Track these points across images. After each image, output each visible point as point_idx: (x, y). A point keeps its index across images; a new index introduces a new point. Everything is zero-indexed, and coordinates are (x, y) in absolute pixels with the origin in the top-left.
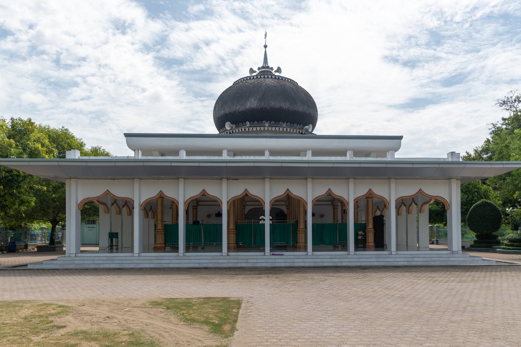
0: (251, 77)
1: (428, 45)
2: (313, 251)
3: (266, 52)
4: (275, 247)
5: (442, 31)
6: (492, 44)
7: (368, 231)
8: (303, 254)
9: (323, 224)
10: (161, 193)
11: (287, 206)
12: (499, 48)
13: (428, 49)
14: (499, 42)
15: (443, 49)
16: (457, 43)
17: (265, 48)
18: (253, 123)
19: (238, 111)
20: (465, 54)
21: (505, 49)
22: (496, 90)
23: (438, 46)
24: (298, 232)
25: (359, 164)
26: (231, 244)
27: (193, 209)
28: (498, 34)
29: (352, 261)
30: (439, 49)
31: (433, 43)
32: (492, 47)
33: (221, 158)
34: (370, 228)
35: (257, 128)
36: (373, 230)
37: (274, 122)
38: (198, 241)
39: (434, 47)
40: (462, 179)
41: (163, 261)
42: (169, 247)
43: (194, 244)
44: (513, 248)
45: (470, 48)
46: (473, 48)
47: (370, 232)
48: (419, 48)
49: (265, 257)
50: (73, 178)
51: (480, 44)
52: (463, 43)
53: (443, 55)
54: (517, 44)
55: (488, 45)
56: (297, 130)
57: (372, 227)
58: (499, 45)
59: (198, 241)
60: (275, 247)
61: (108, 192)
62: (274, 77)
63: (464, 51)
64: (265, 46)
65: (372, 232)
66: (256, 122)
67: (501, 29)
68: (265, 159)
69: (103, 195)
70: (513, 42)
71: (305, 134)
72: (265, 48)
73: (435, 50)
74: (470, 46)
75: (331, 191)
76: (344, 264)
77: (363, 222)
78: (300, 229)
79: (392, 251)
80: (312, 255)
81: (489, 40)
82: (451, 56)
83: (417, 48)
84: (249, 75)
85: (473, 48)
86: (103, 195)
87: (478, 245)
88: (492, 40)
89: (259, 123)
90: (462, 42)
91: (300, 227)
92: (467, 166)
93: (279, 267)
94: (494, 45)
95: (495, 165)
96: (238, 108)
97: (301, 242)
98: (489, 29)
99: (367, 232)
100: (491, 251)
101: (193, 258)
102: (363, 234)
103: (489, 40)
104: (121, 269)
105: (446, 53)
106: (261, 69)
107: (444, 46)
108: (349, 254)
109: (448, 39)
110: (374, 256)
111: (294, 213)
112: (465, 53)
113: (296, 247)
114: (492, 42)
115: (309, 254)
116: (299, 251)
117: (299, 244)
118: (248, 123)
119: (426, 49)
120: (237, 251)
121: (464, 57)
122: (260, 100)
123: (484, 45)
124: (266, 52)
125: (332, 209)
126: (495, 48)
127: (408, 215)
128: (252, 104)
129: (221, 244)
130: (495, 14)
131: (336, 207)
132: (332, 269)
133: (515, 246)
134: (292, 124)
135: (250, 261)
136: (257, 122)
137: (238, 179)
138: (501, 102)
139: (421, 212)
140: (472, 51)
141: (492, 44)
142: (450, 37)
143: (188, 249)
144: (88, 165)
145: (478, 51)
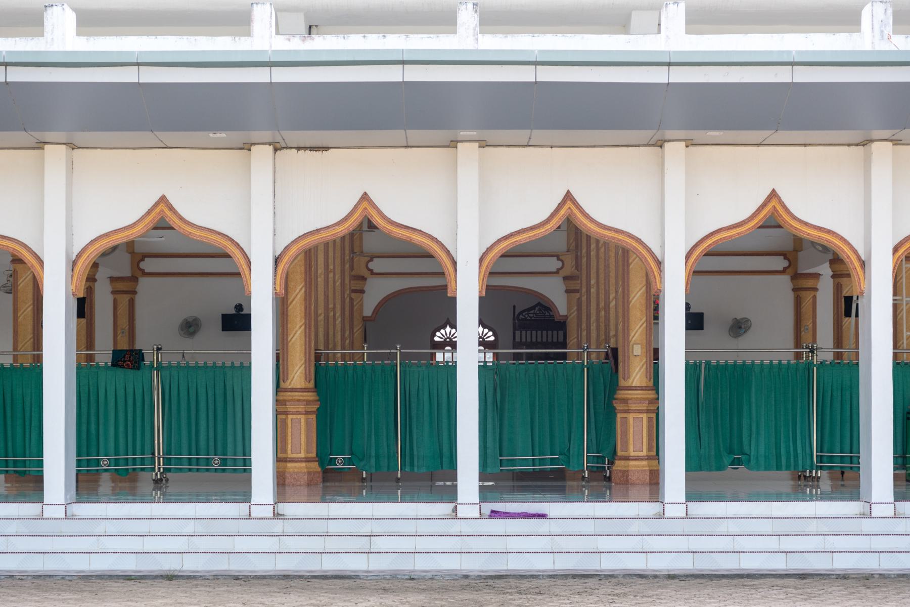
10: (162, 206)
27: (113, 292)
34: (293, 390)
80: (687, 517)
91: (629, 383)
111: (603, 313)
116: (625, 499)
131: (809, 283)
137: (326, 149)
144: (798, 79)
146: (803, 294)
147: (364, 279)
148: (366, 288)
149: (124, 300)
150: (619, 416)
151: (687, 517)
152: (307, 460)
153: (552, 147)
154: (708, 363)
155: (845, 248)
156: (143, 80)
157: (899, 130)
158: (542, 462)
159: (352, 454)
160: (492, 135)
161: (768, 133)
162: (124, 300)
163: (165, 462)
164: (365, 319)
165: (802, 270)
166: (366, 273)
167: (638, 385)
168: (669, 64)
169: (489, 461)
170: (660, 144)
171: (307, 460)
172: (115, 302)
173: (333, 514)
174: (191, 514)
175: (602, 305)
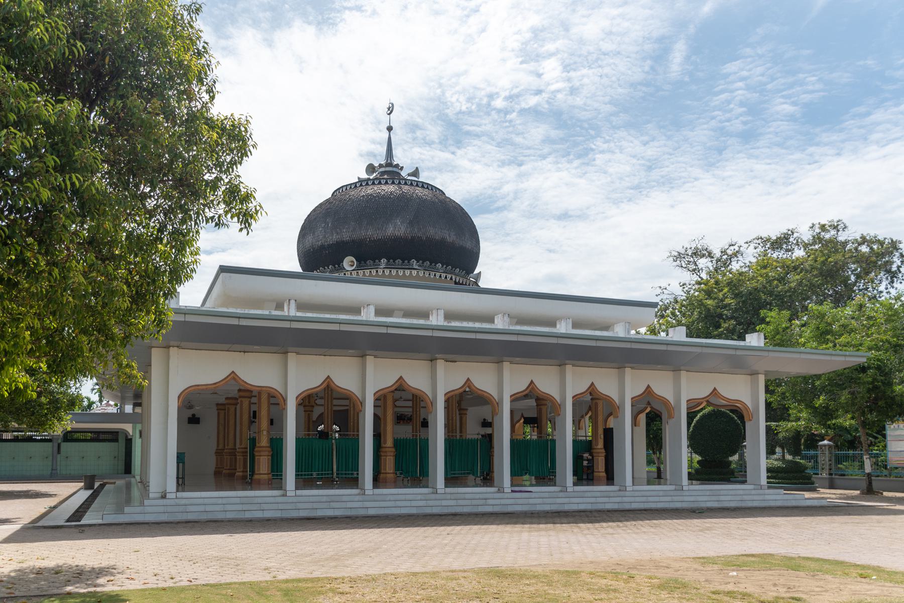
0: (369, 182)
1: (443, 143)
2: (446, 486)
3: (390, 138)
4: (305, 480)
5: (466, 124)
6: (540, 156)
7: (260, 451)
8: (556, 490)
9: (472, 439)
10: (233, 374)
11: (304, 406)
12: (550, 163)
13: (443, 151)
14: (550, 154)
15: (466, 154)
16: (489, 147)
17: (390, 132)
18: (394, 262)
19: (370, 238)
20: (499, 166)
21: (560, 165)
22: (542, 229)
23: (459, 148)
24: (382, 454)
25: (666, 346)
26: (388, 473)
27: (217, 410)
28: (548, 140)
29: (400, 505)
30: (459, 152)
31: (450, 142)
32: (541, 160)
33: (428, 323)
34: (389, 447)
35: (406, 272)
36: (603, 451)
37: (428, 262)
38: (300, 470)
39: (453, 149)
40: (766, 373)
41: (625, 499)
42: (302, 480)
43: (318, 474)
44: (777, 481)
45: (508, 157)
46: (512, 158)
47: (262, 453)
48: (428, 148)
49: (437, 496)
50: (173, 346)
51: (522, 153)
52: (498, 149)
53: (465, 163)
54: (576, 161)
55: (534, 156)
56: (360, 271)
57: (602, 447)
58: (550, 159)
59: (300, 470)
60: (305, 480)
61: (233, 376)
62: (404, 181)
63: (498, 161)
64: (390, 129)
65: (392, 454)
66: (399, 261)
67: (554, 134)
68: (556, 331)
69: (224, 382)
70: (572, 157)
71: (466, 285)
72: (390, 132)
73: (453, 153)
74: (507, 155)
75: (403, 380)
76: (371, 512)
77: (588, 438)
78: (386, 447)
79: (505, 486)
80: (177, 498)
81: (537, 149)
82: (477, 167)
83: (426, 146)
84: (367, 177)
85: (512, 158)
86: (224, 382)
87: (825, 475)
88: (541, 150)
89: (431, 265)
90: (496, 146)
91: (386, 445)
92: (772, 354)
93: (580, 512)
94: (544, 157)
95: (783, 353)
96: (370, 233)
97: (388, 471)
98: (538, 132)
99: (595, 455)
100: (525, 486)
101: (725, 493)
102: (590, 457)
103: (537, 149)
104: (313, 519)
105: (470, 160)
106: (384, 167)
107: (468, 150)
108: (285, 495)
109: (474, 139)
110: (419, 497)
111: (451, 421)
112: (500, 163)
113: (386, 482)
114: (539, 152)
115: (439, 491)
116: (259, 489)
117: (384, 475)
118: (384, 261)
119: (440, 150)
120: (219, 488)
121: (498, 171)
122: (411, 223)
123: (529, 156)
124: (390, 138)
125: (216, 412)
126: (544, 162)
127: (634, 428)
128: (397, 228)
129: (231, 476)
130: (544, 108)
131: (465, 412)
132: (581, 516)
133: (779, 479)
134: (445, 266)
135: (490, 502)
136: (401, 261)
137: (456, 362)
138: (676, 254)
139: (635, 426)
140: (511, 163)
141: (540, 156)
142: (477, 136)
143: (451, 480)
144: (342, 329)
145: (520, 164)
146: (463, 416)
147: (313, 406)
148: (314, 410)
149: (222, 412)
150: (256, 458)
151: (177, 498)
152: (268, 474)
153: (245, 352)
154: (517, 439)
155: (352, 395)
156: (477, 338)
157: (327, 350)
158: (322, 474)
159: (402, 470)
160: (183, 344)
161: (230, 345)
162: (222, 412)
163: (651, 474)
164: (313, 421)
165: (462, 407)
166: (313, 404)
167: (264, 445)
168: (239, 318)
169: (448, 473)
170: (286, 353)
171: (268, 474)
172: (219, 414)
173: (303, 494)
174: (412, 492)
175: (450, 418)
